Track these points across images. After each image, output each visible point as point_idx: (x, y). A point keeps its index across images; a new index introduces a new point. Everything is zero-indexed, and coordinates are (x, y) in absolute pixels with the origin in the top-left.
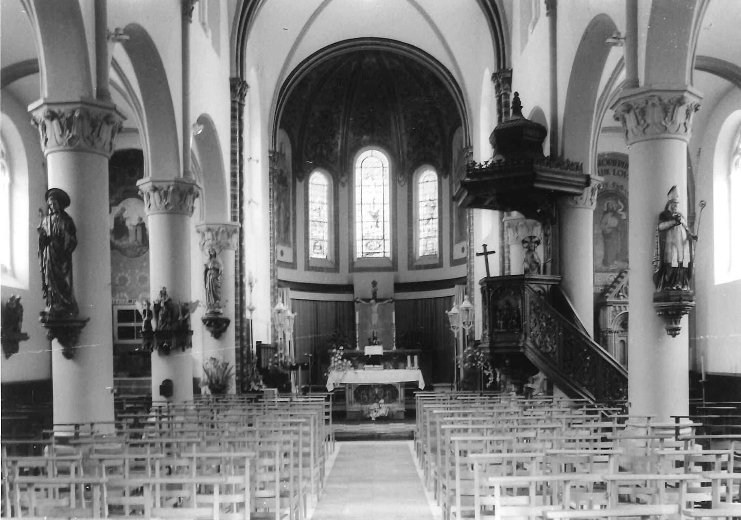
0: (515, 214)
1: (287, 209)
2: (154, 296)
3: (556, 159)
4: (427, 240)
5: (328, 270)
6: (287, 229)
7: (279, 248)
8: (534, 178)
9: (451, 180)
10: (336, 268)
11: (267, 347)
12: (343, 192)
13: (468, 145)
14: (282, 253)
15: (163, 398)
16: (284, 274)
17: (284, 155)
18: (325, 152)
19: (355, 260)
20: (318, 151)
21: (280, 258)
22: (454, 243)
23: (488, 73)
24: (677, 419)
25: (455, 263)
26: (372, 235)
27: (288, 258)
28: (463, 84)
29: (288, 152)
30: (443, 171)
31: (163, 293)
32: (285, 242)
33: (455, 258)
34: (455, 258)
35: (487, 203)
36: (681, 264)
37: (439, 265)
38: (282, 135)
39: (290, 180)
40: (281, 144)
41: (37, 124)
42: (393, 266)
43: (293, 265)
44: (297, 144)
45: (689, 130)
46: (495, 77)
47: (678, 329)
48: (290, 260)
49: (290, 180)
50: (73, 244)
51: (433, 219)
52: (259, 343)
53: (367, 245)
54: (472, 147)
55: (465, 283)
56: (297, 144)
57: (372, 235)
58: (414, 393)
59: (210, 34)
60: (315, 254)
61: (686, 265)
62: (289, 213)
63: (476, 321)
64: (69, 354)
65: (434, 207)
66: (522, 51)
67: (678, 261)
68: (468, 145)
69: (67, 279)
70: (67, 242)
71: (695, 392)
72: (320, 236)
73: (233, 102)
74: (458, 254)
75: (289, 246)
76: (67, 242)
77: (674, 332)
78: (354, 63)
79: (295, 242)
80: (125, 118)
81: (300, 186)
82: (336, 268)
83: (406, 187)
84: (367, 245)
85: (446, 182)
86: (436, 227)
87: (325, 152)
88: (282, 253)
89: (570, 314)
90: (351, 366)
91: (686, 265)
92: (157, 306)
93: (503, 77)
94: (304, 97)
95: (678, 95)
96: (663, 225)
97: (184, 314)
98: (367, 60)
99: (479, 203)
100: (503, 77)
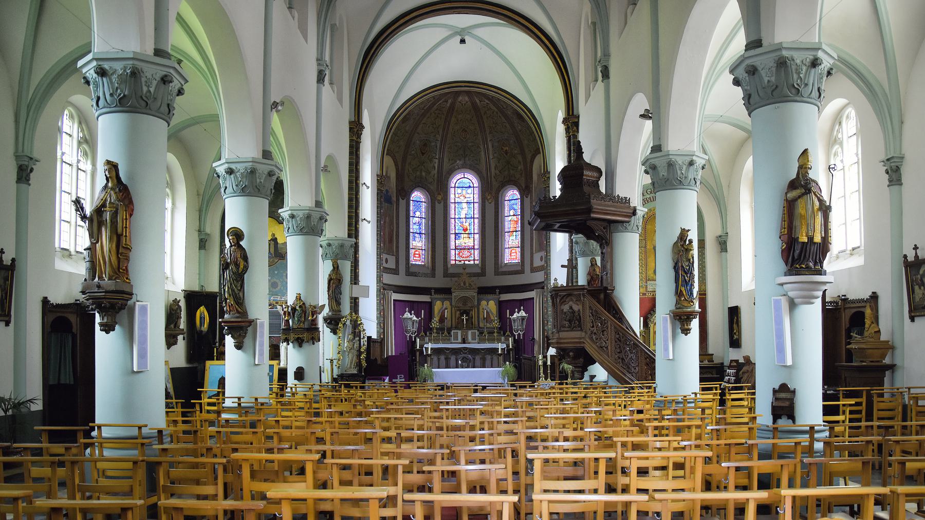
0: (581, 235)
1: (391, 223)
2: (291, 300)
3: (610, 196)
4: (511, 254)
5: (426, 275)
6: (391, 241)
7: (384, 256)
8: (589, 210)
9: (531, 199)
10: (433, 275)
11: (375, 341)
12: (439, 207)
14: (387, 261)
15: (296, 382)
16: (388, 279)
17: (389, 178)
18: (424, 174)
19: (449, 266)
21: (385, 265)
23: (561, 115)
24: (696, 394)
25: (534, 270)
26: (465, 245)
28: (542, 119)
29: (393, 175)
30: (525, 192)
31: (299, 298)
33: (535, 265)
34: (535, 265)
35: (556, 227)
36: (811, 239)
37: (521, 272)
38: (388, 160)
40: (387, 168)
41: (219, 176)
42: (481, 271)
43: (395, 272)
45: (698, 183)
46: (565, 121)
47: (690, 330)
49: (394, 199)
50: (246, 268)
52: (369, 338)
55: (543, 288)
59: (296, 15)
61: (818, 239)
63: (200, 487)
64: (239, 346)
66: (586, 102)
67: (807, 236)
69: (241, 294)
70: (242, 267)
71: (9, 315)
72: (419, 244)
73: (351, 141)
74: (537, 263)
76: (242, 267)
77: (686, 331)
78: (450, 101)
79: (397, 251)
80: (187, 81)
81: (402, 203)
85: (527, 200)
87: (424, 174)
88: (387, 261)
89: (619, 316)
91: (818, 239)
92: (294, 309)
93: (572, 123)
95: (688, 159)
96: (792, 194)
97: (313, 316)
98: (460, 98)
99: (549, 228)
100: (572, 123)
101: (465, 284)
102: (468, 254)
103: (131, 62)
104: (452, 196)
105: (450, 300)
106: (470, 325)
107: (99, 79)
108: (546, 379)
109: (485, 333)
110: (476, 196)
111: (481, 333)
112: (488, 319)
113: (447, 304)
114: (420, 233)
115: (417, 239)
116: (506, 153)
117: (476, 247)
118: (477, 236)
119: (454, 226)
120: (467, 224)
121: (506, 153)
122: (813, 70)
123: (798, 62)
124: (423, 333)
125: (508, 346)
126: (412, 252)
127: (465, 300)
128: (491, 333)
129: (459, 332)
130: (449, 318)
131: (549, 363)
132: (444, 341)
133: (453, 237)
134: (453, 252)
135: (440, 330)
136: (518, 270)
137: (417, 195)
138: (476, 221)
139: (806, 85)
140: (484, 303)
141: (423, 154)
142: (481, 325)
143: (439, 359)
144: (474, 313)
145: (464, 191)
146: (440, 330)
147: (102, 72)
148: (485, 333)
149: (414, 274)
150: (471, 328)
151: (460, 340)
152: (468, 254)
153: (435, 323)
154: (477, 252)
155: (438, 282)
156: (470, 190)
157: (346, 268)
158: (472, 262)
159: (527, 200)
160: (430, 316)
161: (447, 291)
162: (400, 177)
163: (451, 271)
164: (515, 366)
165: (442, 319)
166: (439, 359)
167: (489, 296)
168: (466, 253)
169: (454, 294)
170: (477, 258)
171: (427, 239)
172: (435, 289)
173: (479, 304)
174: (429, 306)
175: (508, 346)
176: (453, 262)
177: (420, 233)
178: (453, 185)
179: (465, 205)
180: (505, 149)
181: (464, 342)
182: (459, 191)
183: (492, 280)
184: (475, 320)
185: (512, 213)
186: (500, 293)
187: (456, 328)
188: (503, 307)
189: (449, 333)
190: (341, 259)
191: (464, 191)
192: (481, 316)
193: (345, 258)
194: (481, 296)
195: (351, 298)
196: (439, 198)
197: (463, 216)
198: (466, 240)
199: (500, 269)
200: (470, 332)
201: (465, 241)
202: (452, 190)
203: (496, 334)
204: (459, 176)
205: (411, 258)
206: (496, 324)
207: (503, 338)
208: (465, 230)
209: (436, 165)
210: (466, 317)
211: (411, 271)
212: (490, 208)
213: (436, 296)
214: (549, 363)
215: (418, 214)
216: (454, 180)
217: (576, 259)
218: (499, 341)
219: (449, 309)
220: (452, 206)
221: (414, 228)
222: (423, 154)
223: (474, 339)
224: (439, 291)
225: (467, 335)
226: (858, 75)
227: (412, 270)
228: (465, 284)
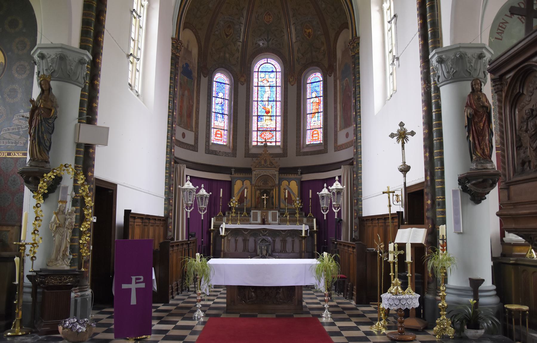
1: (191, 98)
6: (190, 116)
7: (179, 131)
10: (234, 153)
12: (242, 89)
13: (354, 35)
17: (190, 53)
18: (227, 55)
19: (250, 147)
20: (222, 54)
22: (338, 130)
25: (338, 148)
26: (267, 127)
27: (190, 139)
32: (188, 126)
39: (195, 74)
43: (194, 148)
44: (203, 43)
48: (192, 143)
49: (195, 74)
51: (318, 112)
52: (127, 213)
53: (261, 136)
54: (359, 38)
56: (203, 43)
57: (267, 127)
58: (120, 218)
60: (214, 139)
62: (193, 102)
65: (319, 104)
68: (354, 35)
72: (222, 125)
75: (192, 131)
81: (204, 80)
82: (234, 153)
83: (296, 85)
84: (261, 136)
85: (331, 79)
86: (321, 118)
87: (227, 55)
90: (32, 101)
94: (210, 6)
95: (478, 52)
101: (265, 161)
102: (270, 136)
103: (60, 50)
104: (255, 80)
105: (250, 179)
106: (271, 206)
107: (41, 61)
108: (404, 287)
109: (287, 213)
110: (279, 81)
111: (282, 214)
112: (290, 200)
113: (247, 183)
114: (222, 114)
115: (219, 119)
116: (309, 36)
117: (278, 129)
118: (279, 119)
119: (257, 109)
120: (269, 107)
121: (309, 36)
122: (480, 60)
123: (469, 55)
124: (221, 213)
125: (311, 227)
126: (213, 131)
127: (265, 179)
128: (292, 213)
129: (259, 213)
130: (249, 198)
131: (409, 259)
132: (243, 222)
133: (255, 119)
134: (254, 134)
135: (239, 210)
136: (320, 150)
137: (220, 77)
138: (279, 104)
139: (475, 70)
140: (285, 183)
141: (227, 36)
142: (282, 206)
143: (236, 241)
144: (275, 192)
145: (267, 74)
146: (239, 210)
147: (42, 57)
148: (287, 213)
149: (215, 153)
150: (272, 209)
151: (259, 220)
152: (270, 136)
153: (234, 203)
154: (279, 135)
155: (239, 162)
156: (273, 75)
157: (72, 97)
158: (274, 144)
159: (331, 79)
160: (229, 194)
161: (247, 171)
162: (202, 54)
163: (252, 151)
164: (335, 259)
165: (241, 200)
166: (236, 241)
167: (292, 176)
168: (268, 135)
169: (254, 173)
170: (278, 140)
171: (230, 119)
172: (235, 168)
173: (280, 184)
174: (229, 186)
175: (311, 227)
176: (254, 144)
177: (222, 114)
178: (257, 70)
179: (267, 89)
180: (308, 31)
181: (264, 222)
182: (262, 75)
183: (294, 160)
184: (275, 200)
185: (314, 95)
186: (301, 174)
187: (256, 208)
188: (303, 186)
189: (249, 214)
190: (59, 79)
191: (267, 74)
192: (282, 197)
193: (68, 77)
194: (283, 176)
195: (78, 145)
196: (243, 79)
197: (266, 99)
198: (268, 122)
199: (302, 150)
200: (270, 213)
201: (267, 123)
202: (255, 75)
203: (297, 215)
204: (262, 62)
205: (213, 137)
206: (297, 204)
207: (305, 220)
208: (268, 112)
209: (240, 48)
210: (266, 198)
211: (210, 149)
212: (293, 89)
213: (236, 175)
214: (409, 259)
215: (221, 95)
216: (258, 65)
217: (437, 90)
218: (301, 223)
219: (249, 189)
220: (255, 89)
221: (216, 107)
222: (227, 36)
223: (274, 219)
224: (239, 170)
225: (267, 216)
226: (499, 66)
227: (213, 148)
228: (265, 161)
